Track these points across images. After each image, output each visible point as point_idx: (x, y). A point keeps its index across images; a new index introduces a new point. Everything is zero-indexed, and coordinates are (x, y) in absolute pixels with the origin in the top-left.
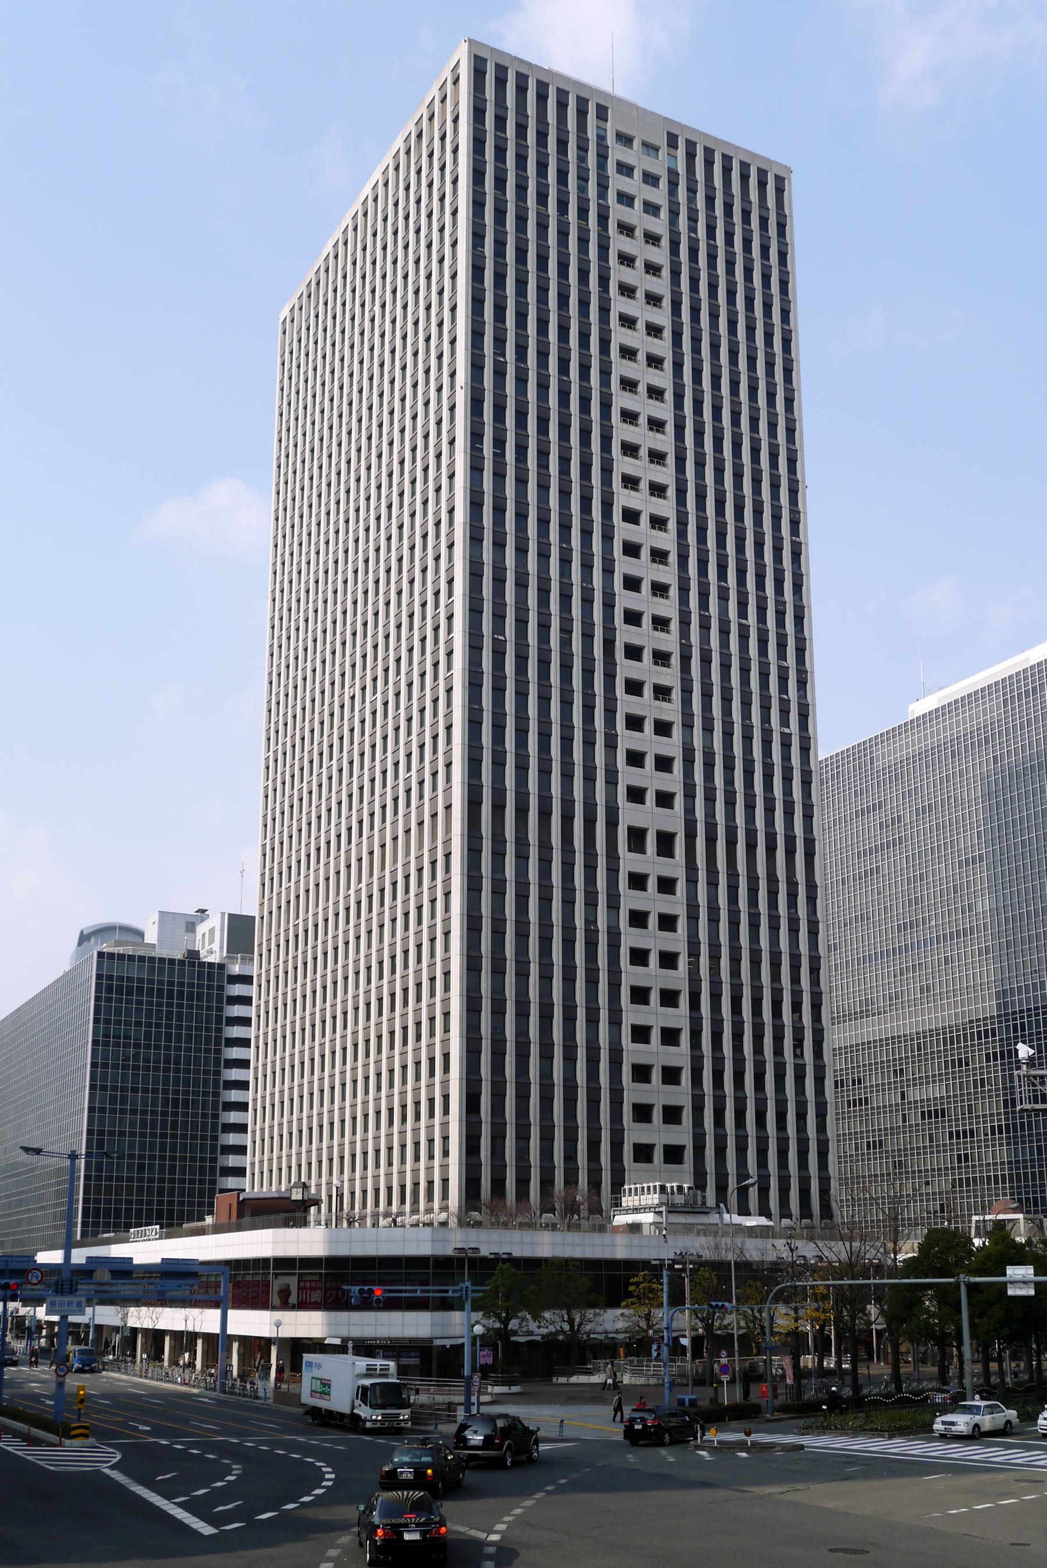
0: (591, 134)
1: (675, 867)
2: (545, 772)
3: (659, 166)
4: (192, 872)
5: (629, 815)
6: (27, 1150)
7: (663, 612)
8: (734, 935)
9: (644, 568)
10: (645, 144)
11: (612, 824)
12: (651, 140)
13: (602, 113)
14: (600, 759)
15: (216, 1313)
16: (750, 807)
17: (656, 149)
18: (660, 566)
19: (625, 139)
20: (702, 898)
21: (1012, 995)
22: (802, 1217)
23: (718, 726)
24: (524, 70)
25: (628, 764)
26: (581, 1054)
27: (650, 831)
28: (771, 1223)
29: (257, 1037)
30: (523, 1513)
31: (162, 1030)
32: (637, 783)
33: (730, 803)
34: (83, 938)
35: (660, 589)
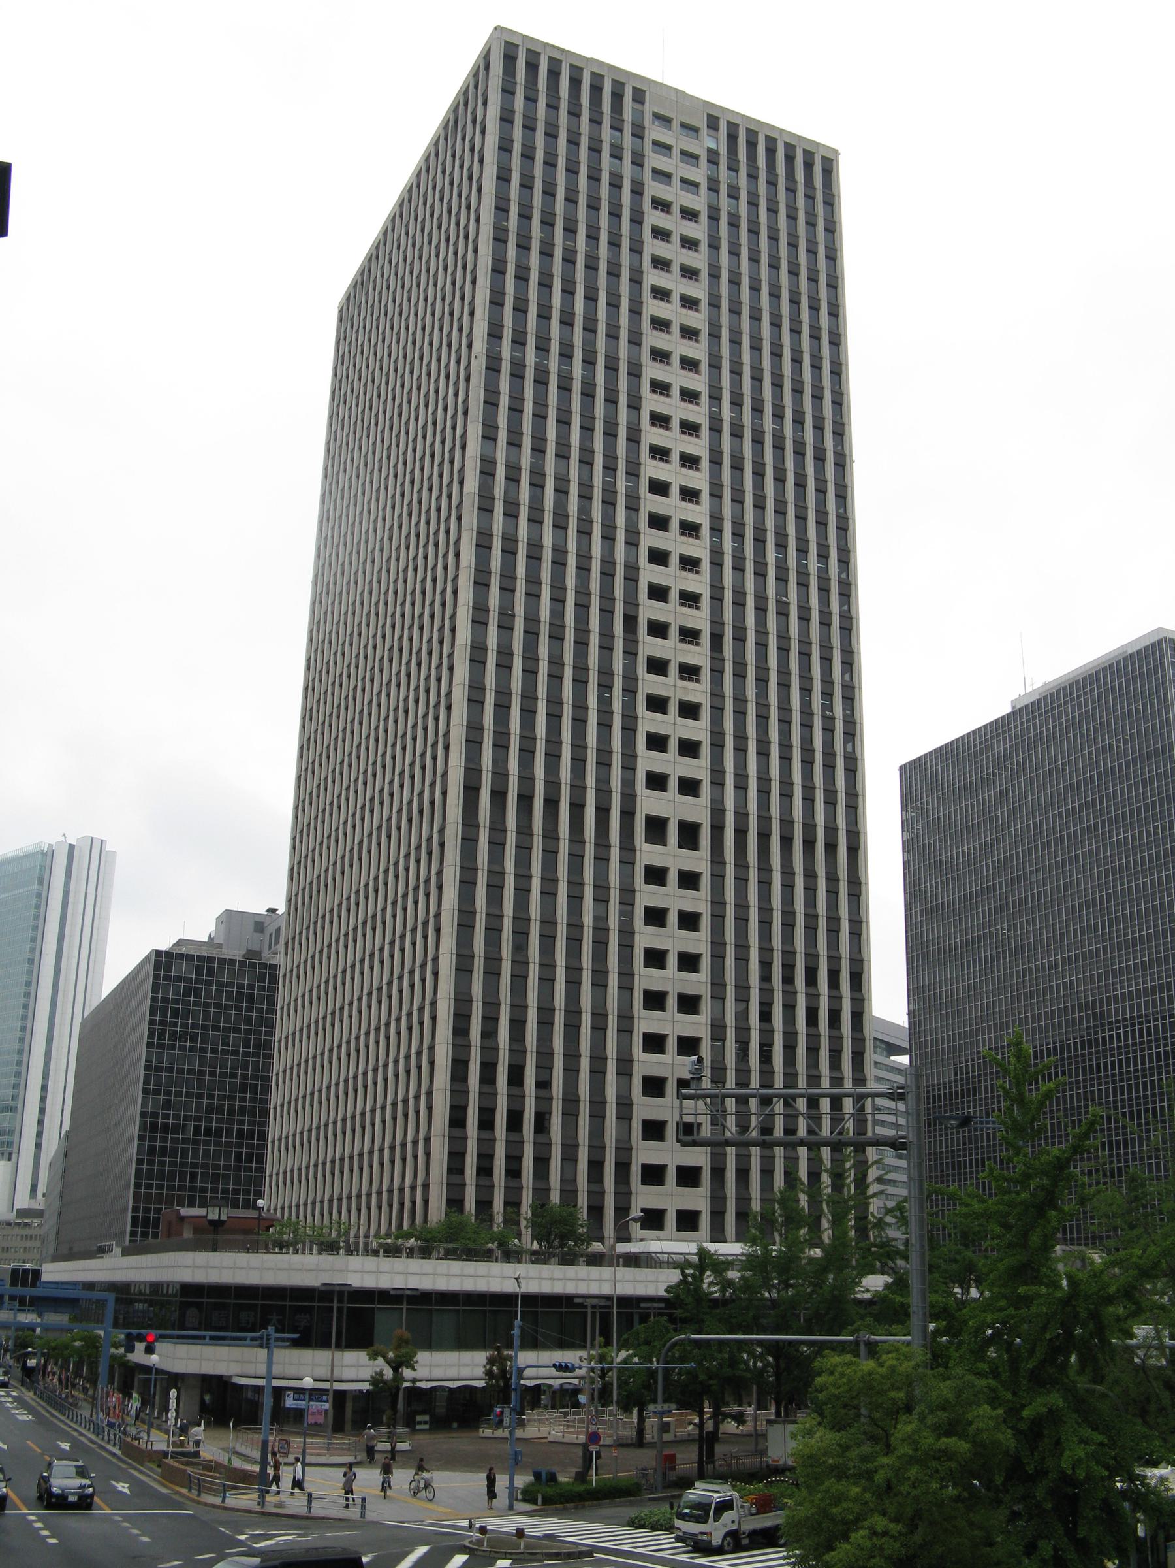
1: (699, 861)
2: (549, 894)
5: (649, 803)
10: (684, 125)
13: (639, 96)
16: (786, 758)
17: (696, 130)
19: (665, 121)
21: (1109, 1004)
24: (556, 55)
26: (585, 1064)
27: (671, 912)
32: (657, 862)
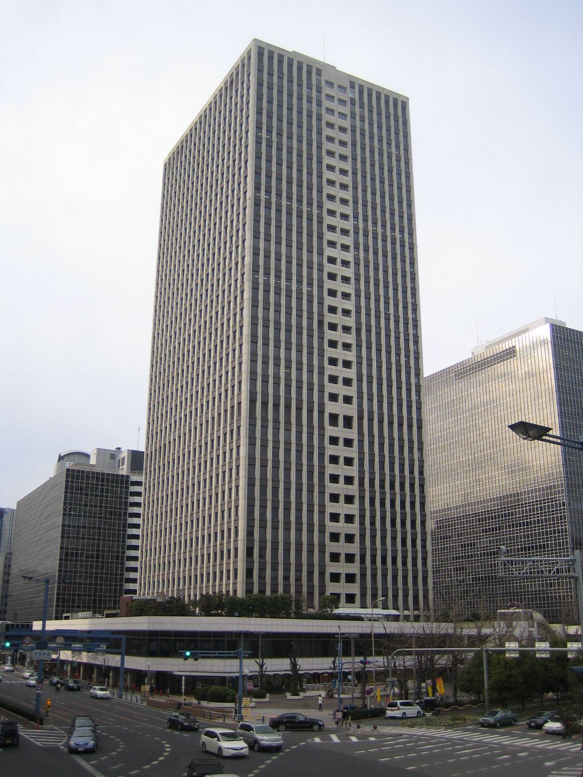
0: (314, 82)
3: (346, 97)
4: (115, 420)
6: (25, 578)
7: (347, 307)
8: (380, 390)
9: (340, 371)
11: (321, 412)
12: (341, 84)
13: (319, 72)
14: (316, 362)
15: (119, 657)
17: (345, 89)
18: (346, 285)
19: (330, 84)
20: (364, 371)
22: (414, 610)
23: (374, 363)
25: (329, 382)
27: (340, 378)
28: (398, 613)
29: (140, 578)
30: (271, 763)
31: (95, 495)
33: (380, 402)
34: (61, 458)
35: (346, 296)
